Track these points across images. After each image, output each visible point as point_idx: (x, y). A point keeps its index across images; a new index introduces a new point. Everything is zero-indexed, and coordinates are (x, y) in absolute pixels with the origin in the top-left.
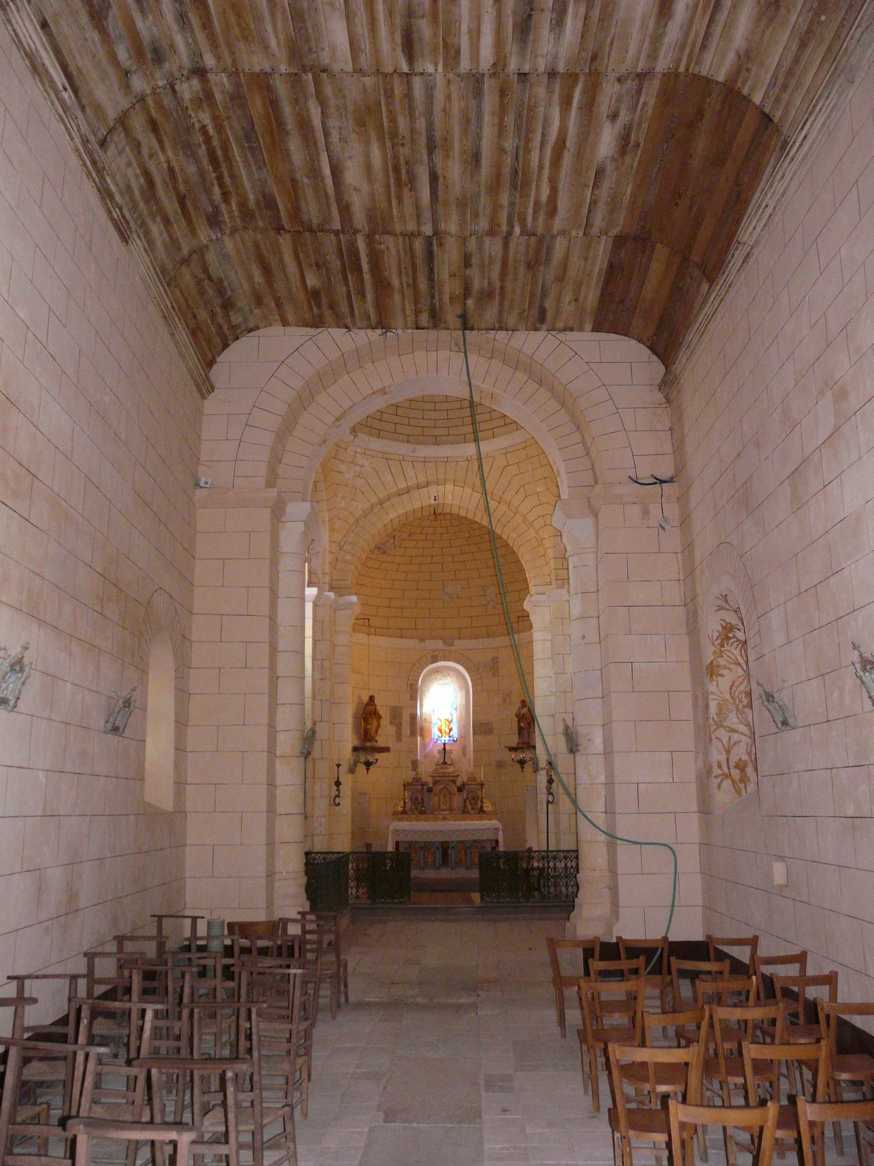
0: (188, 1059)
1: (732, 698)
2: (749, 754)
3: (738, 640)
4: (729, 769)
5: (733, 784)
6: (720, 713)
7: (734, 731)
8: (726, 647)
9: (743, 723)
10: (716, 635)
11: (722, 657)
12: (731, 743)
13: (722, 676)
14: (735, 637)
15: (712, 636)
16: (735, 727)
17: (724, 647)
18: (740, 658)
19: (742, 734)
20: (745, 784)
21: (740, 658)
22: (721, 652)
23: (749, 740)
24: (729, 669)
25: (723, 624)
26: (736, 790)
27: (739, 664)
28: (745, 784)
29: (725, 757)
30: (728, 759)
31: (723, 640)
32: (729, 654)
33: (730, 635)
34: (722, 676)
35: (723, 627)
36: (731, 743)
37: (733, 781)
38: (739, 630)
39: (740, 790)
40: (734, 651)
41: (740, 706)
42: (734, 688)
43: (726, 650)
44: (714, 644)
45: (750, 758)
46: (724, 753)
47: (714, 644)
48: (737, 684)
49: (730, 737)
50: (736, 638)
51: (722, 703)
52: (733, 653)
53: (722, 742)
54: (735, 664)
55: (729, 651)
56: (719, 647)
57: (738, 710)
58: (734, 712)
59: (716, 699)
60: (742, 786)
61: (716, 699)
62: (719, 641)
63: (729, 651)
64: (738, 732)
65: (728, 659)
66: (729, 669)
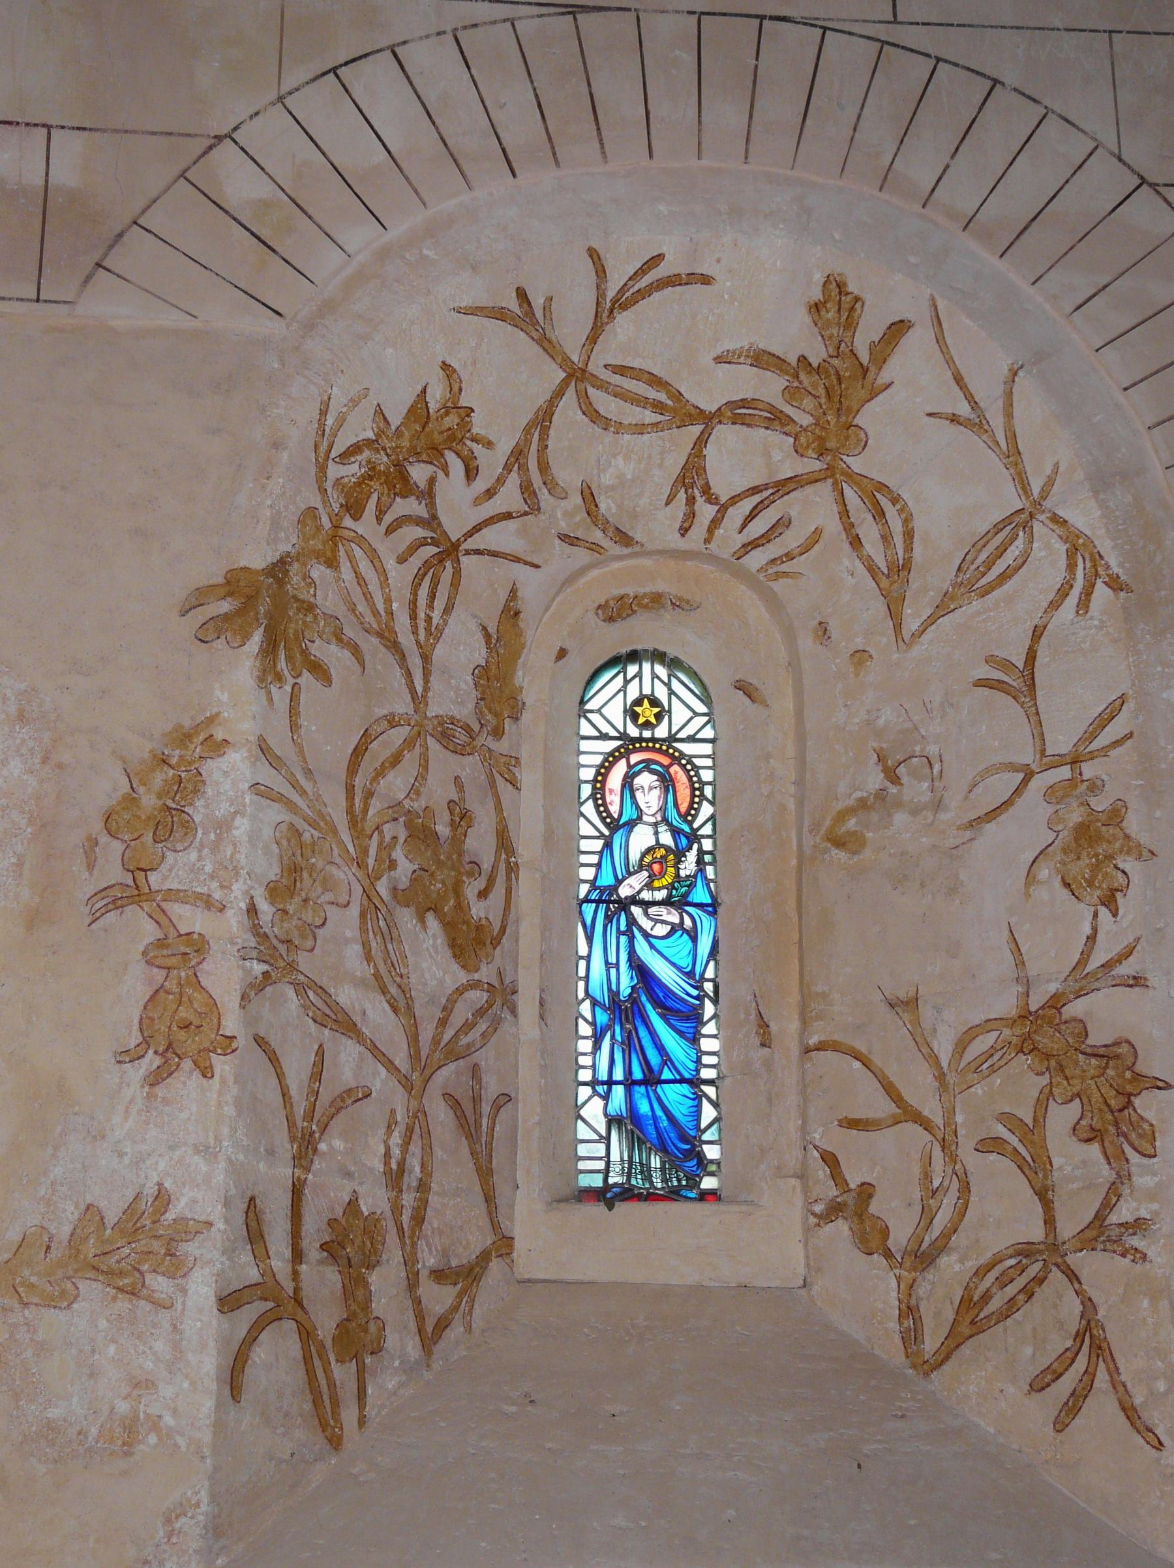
0: (398, 45)
1: (354, 822)
2: (395, 1178)
3: (432, 521)
4: (298, 1255)
5: (307, 1360)
6: (291, 891)
7: (346, 1025)
8: (366, 526)
9: (384, 991)
10: (360, 428)
11: (332, 563)
12: (325, 1097)
13: (319, 670)
14: (428, 494)
15: (341, 421)
16: (346, 996)
17: (356, 517)
18: (402, 621)
19: (375, 1051)
20: (361, 1370)
21: (402, 621)
22: (335, 537)
23: (400, 1102)
24: (356, 651)
25: (436, 397)
26: (317, 1402)
27: (394, 646)
28: (361, 1370)
29: (285, 1172)
30: (297, 1191)
31: (372, 473)
32: (364, 566)
33: (419, 473)
34: (319, 670)
35: (419, 410)
36: (325, 1097)
37: (306, 1334)
38: (471, 473)
39: (336, 1403)
40: (390, 564)
41: (383, 888)
42: (368, 766)
43: (361, 540)
44: (322, 469)
45: (396, 1209)
46: (286, 1148)
47: (322, 469)
48: (379, 751)
49: (321, 1052)
50: (431, 505)
51: (309, 834)
52: (383, 573)
53: (280, 1076)
54: (380, 635)
55: (373, 556)
56: (336, 500)
57: (371, 907)
58: (355, 910)
59: (279, 798)
60: (345, 1374)
61: (279, 798)
62: (353, 470)
63: (373, 556)
64: (360, 1038)
65: (357, 594)
66: (356, 651)
